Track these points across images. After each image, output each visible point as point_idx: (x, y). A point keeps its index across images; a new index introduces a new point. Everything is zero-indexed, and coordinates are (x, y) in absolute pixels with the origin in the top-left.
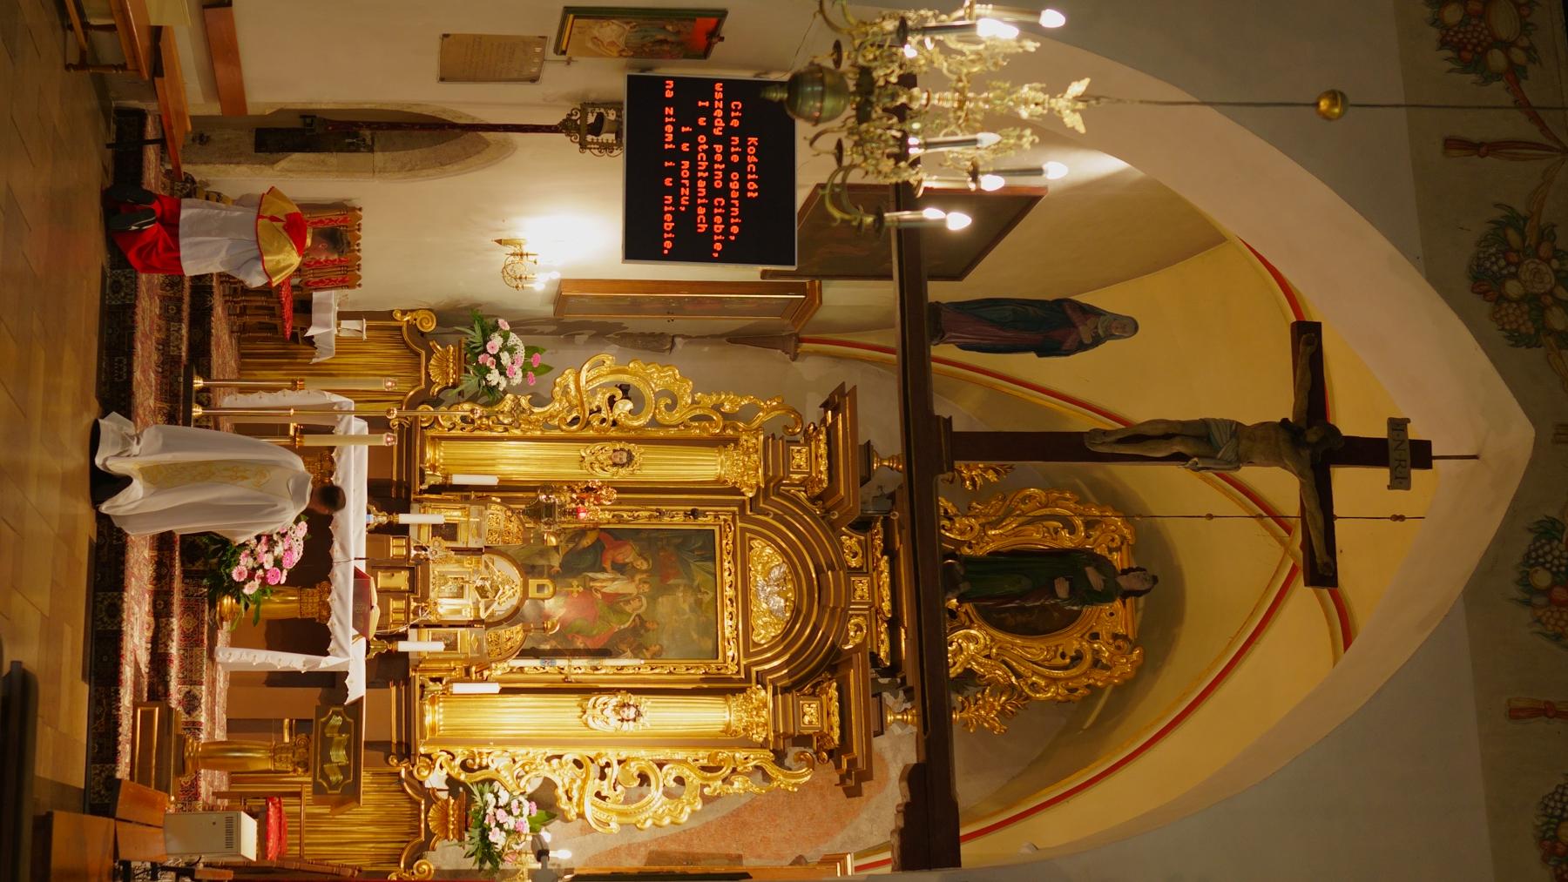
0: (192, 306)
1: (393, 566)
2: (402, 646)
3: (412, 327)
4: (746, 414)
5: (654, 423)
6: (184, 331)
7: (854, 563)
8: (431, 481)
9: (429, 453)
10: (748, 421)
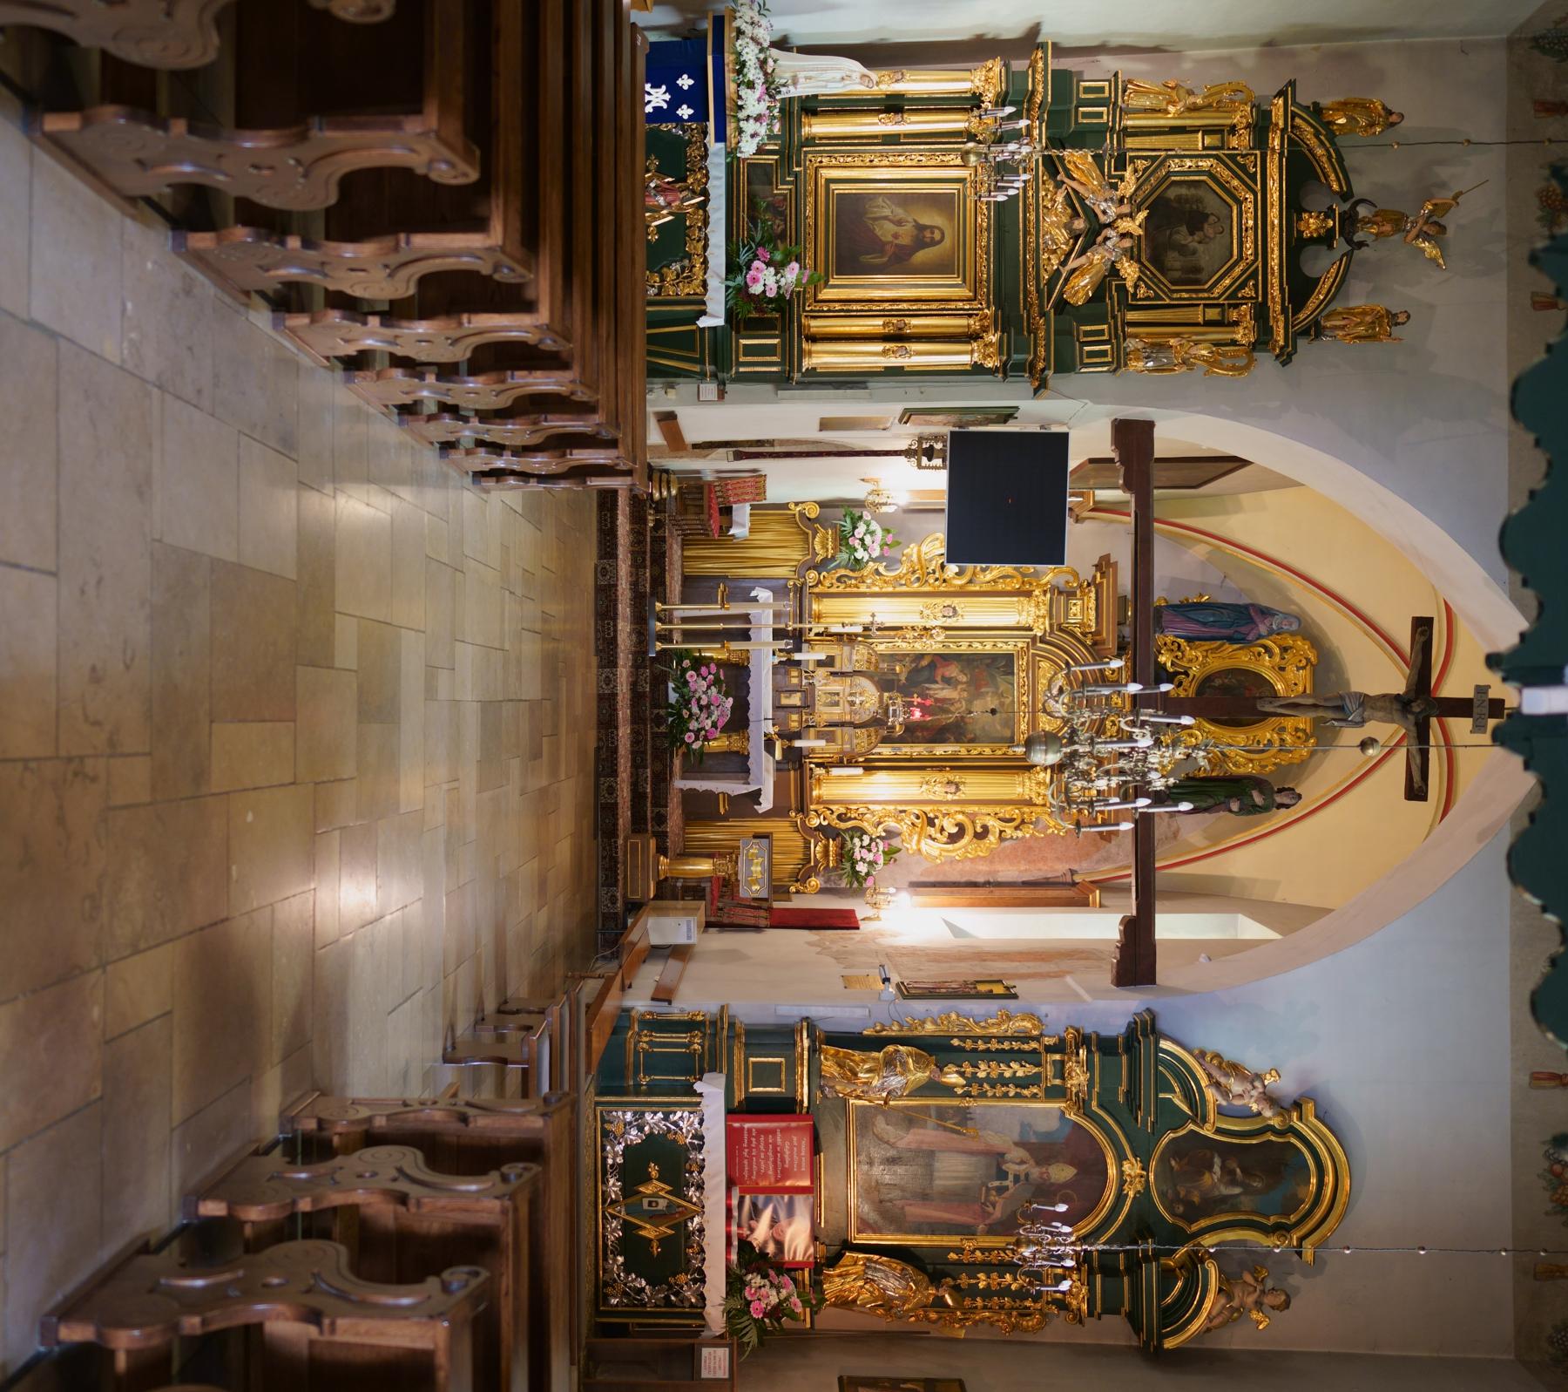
2: (798, 743)
3: (802, 515)
9: (815, 607)
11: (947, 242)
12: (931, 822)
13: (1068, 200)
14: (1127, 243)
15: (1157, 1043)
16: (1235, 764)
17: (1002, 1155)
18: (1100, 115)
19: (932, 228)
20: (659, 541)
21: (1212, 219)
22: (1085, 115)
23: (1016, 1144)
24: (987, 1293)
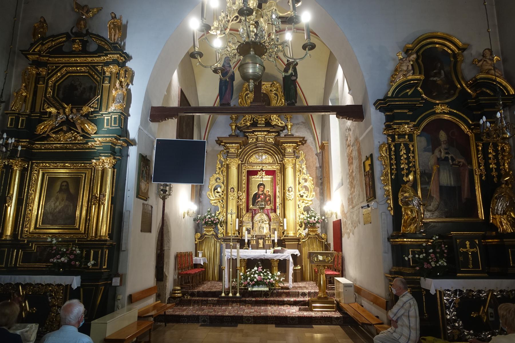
0: (202, 297)
1: (258, 243)
2: (276, 241)
3: (199, 239)
4: (221, 162)
5: (223, 183)
6: (210, 299)
7: (255, 140)
8: (238, 234)
10: (223, 162)
11: (67, 180)
12: (302, 196)
13: (56, 133)
14: (74, 110)
15: (389, 97)
16: (282, 104)
17: (438, 159)
18: (23, 120)
19: (61, 186)
20: (199, 294)
21: (73, 82)
22: (22, 125)
23: (433, 153)
24: (498, 164)
